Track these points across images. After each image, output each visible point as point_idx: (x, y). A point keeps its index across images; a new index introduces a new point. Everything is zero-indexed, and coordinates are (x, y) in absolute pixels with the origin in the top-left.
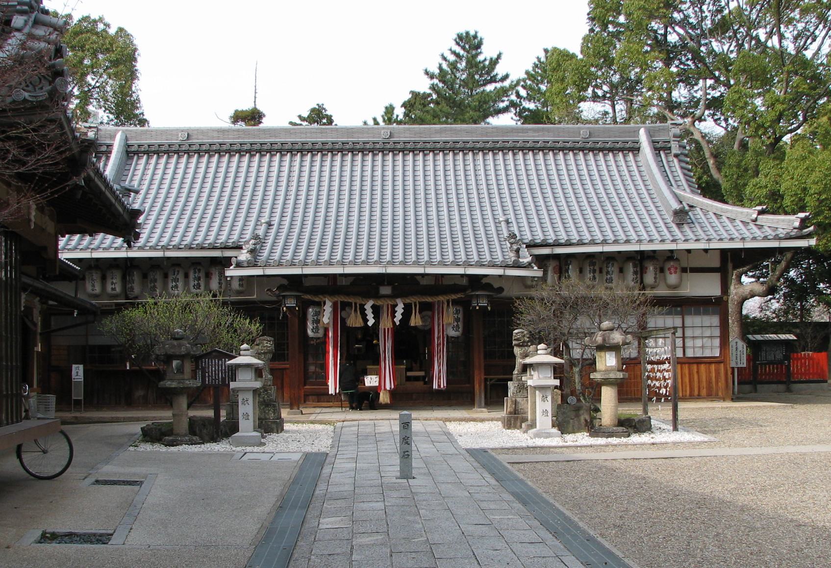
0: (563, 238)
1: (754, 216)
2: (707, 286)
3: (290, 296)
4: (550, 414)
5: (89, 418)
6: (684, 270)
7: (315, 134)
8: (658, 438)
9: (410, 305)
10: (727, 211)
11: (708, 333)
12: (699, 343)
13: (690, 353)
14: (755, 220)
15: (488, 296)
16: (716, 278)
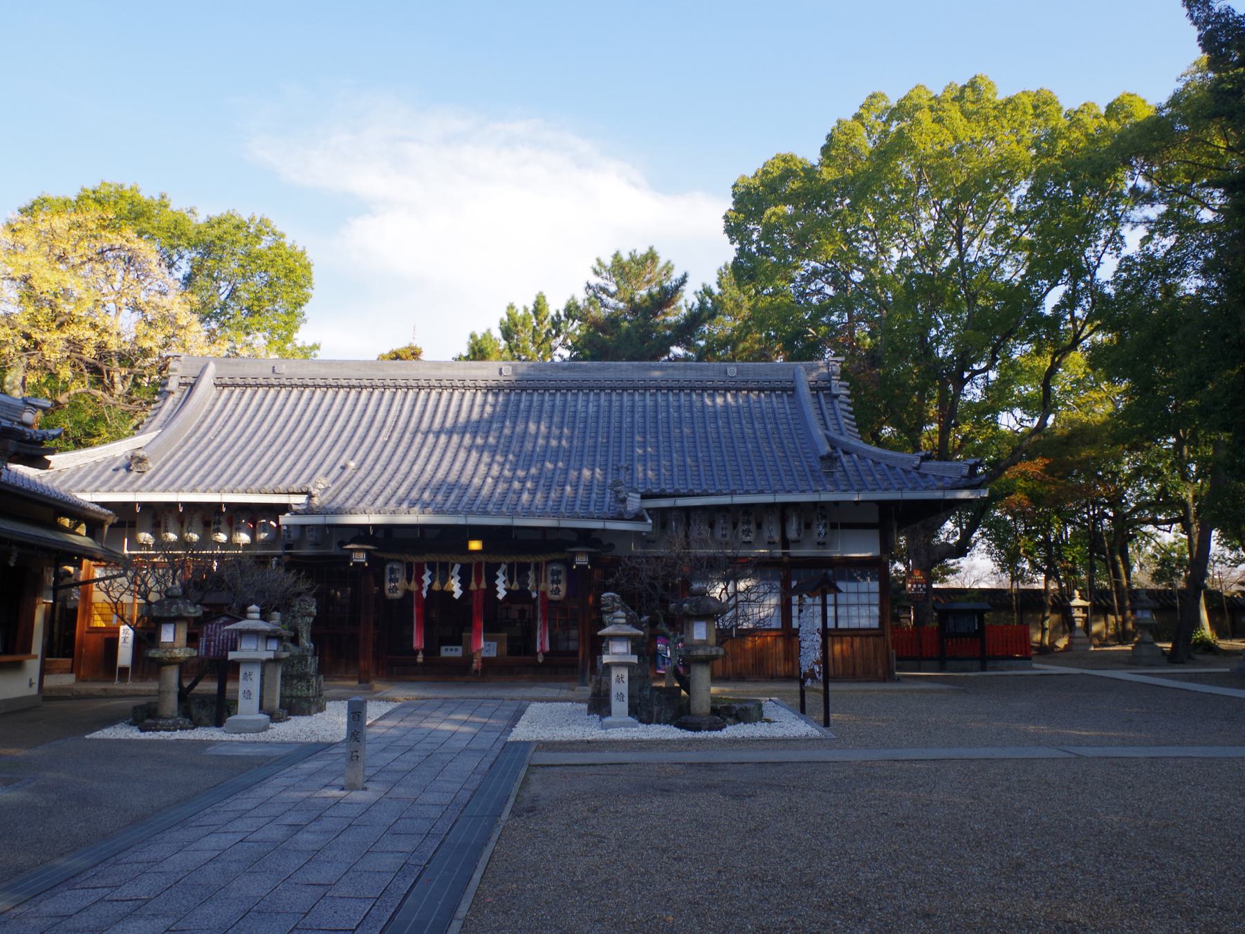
0: (680, 487)
1: (918, 462)
2: (862, 549)
3: (582, 553)
4: (626, 699)
5: (122, 691)
6: (834, 526)
7: (401, 371)
8: (776, 731)
9: (470, 565)
10: (885, 457)
11: (864, 599)
12: (854, 611)
13: (842, 625)
14: (917, 468)
15: (367, 551)
16: (874, 536)
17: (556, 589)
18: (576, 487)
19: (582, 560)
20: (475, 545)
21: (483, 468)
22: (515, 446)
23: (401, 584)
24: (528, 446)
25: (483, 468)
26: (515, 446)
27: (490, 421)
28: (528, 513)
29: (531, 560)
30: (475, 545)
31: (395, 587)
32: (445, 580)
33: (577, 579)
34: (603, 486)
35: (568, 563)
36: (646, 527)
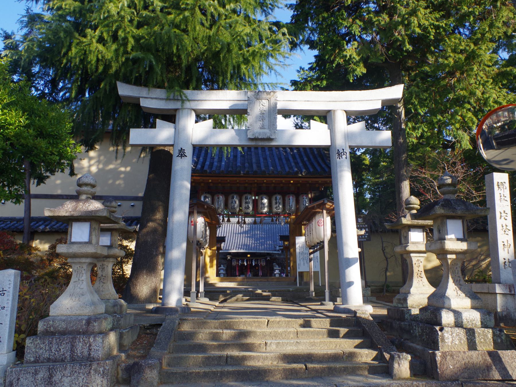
17: (263, 264)
18: (269, 245)
19: (268, 258)
20: (249, 256)
21: (251, 241)
22: (254, 237)
23: (235, 263)
24: (256, 237)
25: (251, 241)
26: (254, 237)
27: (248, 231)
28: (262, 250)
29: (259, 258)
30: (249, 256)
31: (234, 263)
32: (243, 262)
33: (267, 261)
34: (272, 245)
35: (266, 259)
36: (280, 252)
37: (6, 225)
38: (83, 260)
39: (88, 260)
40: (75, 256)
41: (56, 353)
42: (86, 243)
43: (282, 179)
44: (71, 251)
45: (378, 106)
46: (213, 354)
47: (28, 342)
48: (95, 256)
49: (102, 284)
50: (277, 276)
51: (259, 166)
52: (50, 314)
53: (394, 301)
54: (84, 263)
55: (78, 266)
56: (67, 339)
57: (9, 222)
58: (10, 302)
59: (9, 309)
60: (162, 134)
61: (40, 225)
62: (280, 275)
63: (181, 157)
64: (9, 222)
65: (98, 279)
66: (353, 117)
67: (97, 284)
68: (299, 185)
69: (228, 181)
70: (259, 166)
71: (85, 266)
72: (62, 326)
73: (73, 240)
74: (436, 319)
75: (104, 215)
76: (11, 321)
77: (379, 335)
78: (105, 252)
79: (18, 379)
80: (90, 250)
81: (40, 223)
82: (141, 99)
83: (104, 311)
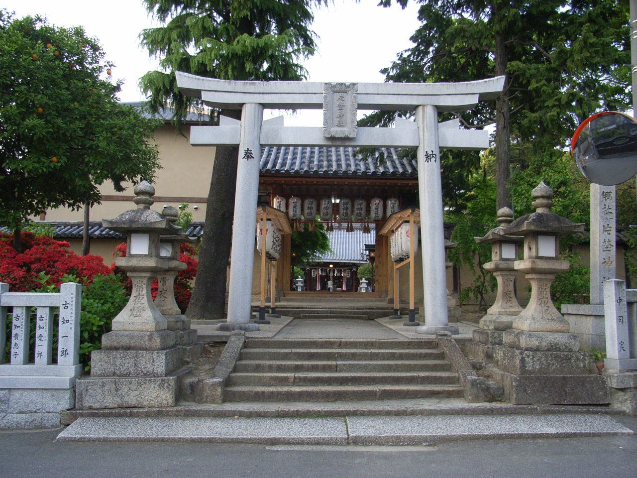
30: (331, 266)
35: (351, 270)
37: (60, 230)
38: (144, 274)
39: (148, 275)
40: (135, 269)
41: (121, 367)
42: (146, 256)
43: (366, 181)
44: (130, 264)
45: (475, 100)
46: (439, 407)
47: (95, 356)
48: (154, 271)
49: (163, 299)
50: (364, 291)
51: (339, 166)
52: (113, 329)
53: (480, 323)
54: (145, 277)
55: (138, 280)
56: (132, 353)
57: (62, 227)
58: (74, 316)
59: (73, 322)
60: (226, 131)
61: (95, 231)
62: (367, 289)
63: (248, 158)
64: (62, 227)
65: (159, 293)
66: (444, 114)
67: (157, 300)
68: (386, 188)
69: (304, 182)
70: (339, 166)
71: (145, 281)
72: (125, 341)
73: (133, 252)
74: (519, 342)
75: (164, 227)
76: (75, 333)
77: (459, 358)
78: (166, 266)
79: (87, 390)
80: (151, 263)
81: (95, 228)
82: (202, 92)
83: (166, 328)
